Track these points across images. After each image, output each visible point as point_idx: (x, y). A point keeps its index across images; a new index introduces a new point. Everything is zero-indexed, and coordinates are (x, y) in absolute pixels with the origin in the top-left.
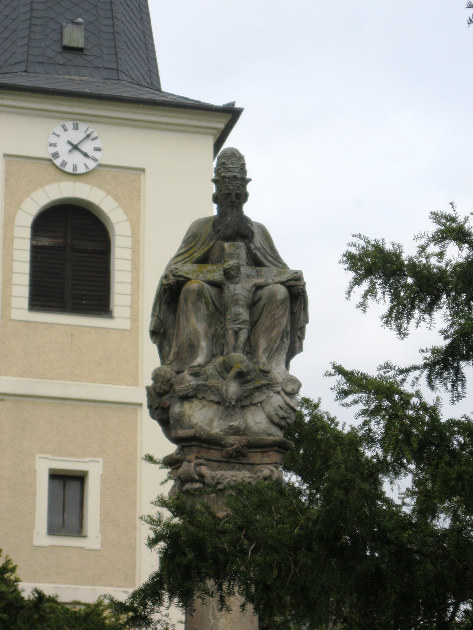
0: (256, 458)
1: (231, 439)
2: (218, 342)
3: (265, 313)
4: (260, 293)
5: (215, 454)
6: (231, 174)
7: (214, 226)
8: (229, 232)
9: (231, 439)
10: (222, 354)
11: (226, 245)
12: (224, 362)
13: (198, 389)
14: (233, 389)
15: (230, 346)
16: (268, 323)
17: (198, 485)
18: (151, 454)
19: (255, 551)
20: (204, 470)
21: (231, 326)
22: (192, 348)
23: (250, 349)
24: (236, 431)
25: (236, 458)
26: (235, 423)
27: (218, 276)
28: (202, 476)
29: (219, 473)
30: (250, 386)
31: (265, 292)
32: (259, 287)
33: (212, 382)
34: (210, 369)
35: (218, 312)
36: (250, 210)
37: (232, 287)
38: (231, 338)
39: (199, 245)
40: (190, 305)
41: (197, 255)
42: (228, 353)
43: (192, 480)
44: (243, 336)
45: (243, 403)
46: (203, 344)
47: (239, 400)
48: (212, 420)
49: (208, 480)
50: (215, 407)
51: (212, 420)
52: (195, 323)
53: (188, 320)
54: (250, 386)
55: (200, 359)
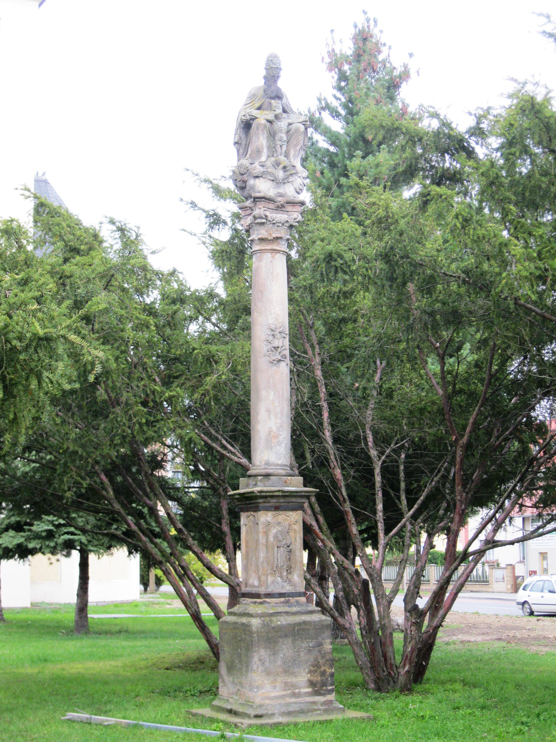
0: (289, 208)
1: (279, 199)
2: (272, 150)
3: (293, 137)
4: (290, 127)
5: (271, 206)
6: (275, 66)
7: (265, 91)
8: (273, 95)
9: (279, 199)
10: (273, 156)
11: (273, 101)
12: (276, 160)
13: (263, 173)
14: (281, 174)
15: (279, 153)
16: (295, 143)
17: (264, 221)
18: (194, 200)
19: (359, 260)
20: (268, 213)
21: (279, 143)
22: (259, 152)
23: (287, 155)
24: (281, 195)
25: (281, 208)
26: (280, 191)
27: (271, 117)
28: (266, 216)
29: (274, 215)
30: (288, 173)
31: (293, 126)
32: (290, 124)
33: (270, 170)
34: (269, 163)
35: (272, 135)
36: (281, 84)
37: (279, 123)
38: (279, 149)
39: (257, 100)
40: (260, 131)
41: (257, 105)
42: (277, 156)
43: (262, 218)
44: (284, 148)
45: (285, 181)
46: (265, 150)
47: (283, 180)
48: (269, 189)
49: (269, 218)
50: (271, 182)
51: (269, 189)
52: (260, 140)
53: (258, 138)
54: (288, 173)
55: (263, 158)
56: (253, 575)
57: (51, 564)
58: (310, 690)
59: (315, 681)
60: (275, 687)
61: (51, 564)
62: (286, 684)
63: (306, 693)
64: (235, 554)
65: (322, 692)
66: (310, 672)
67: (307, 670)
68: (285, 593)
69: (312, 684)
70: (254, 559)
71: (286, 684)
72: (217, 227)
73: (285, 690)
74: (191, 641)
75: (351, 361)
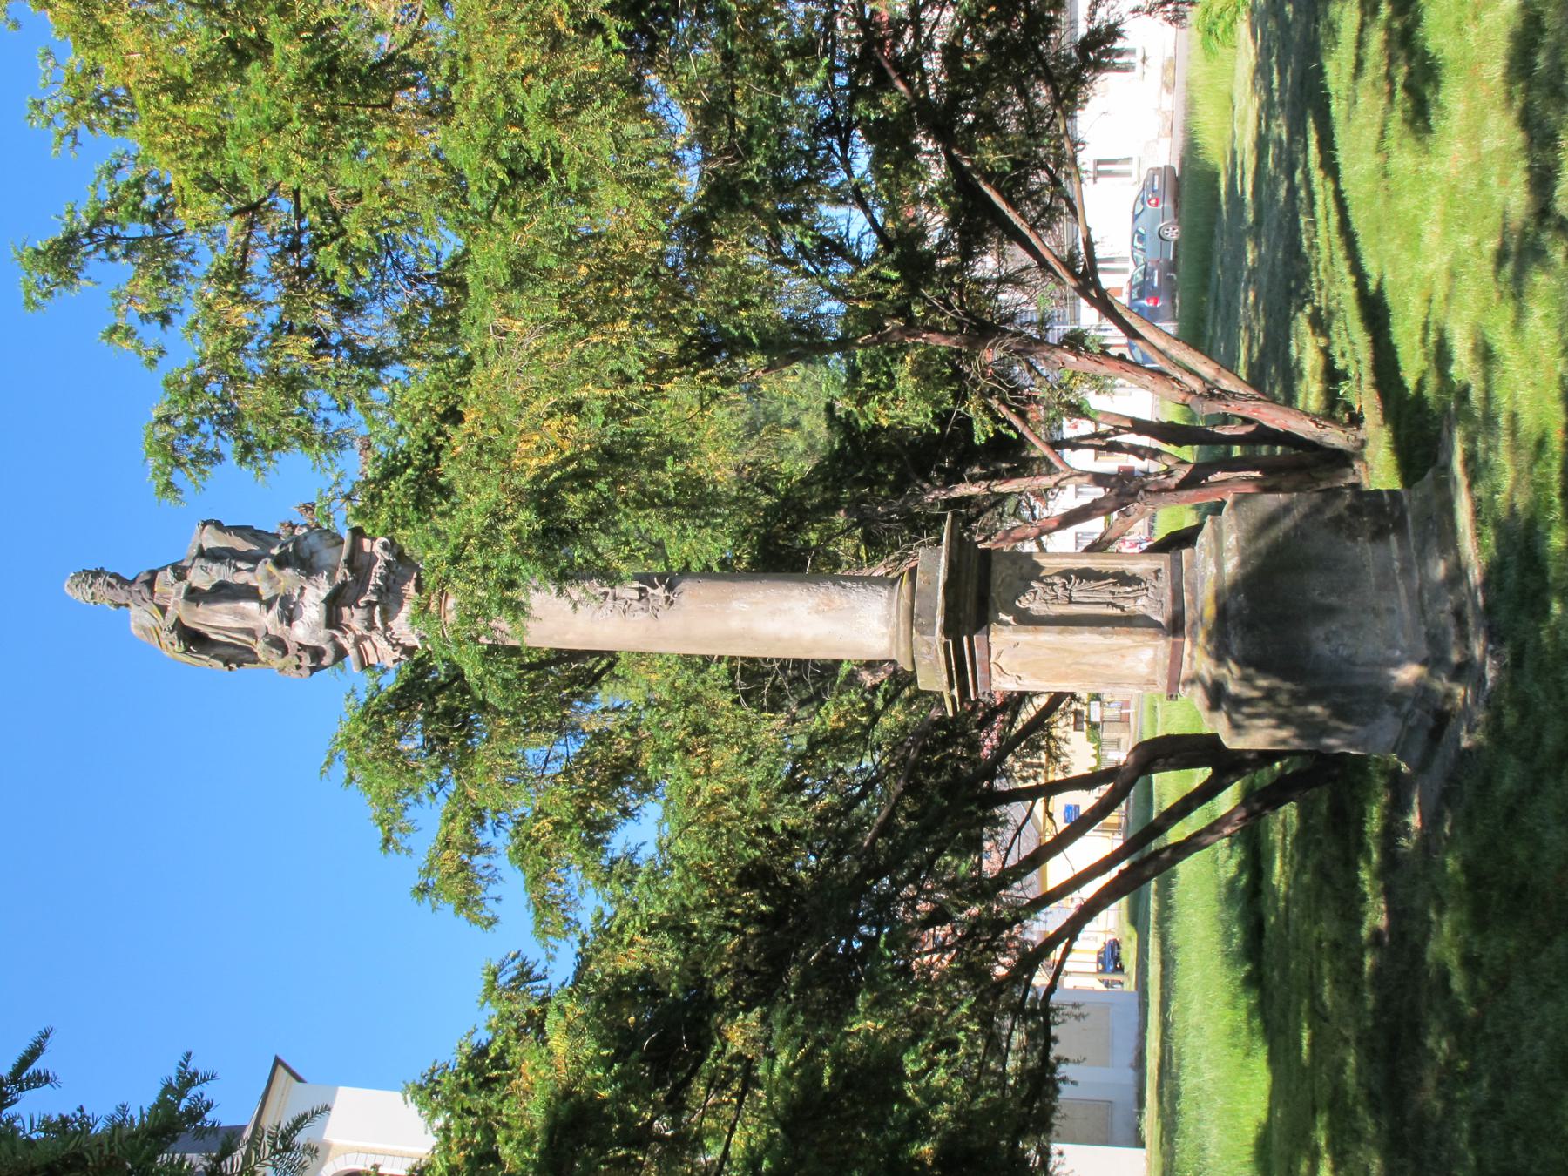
56: (1129, 662)
57: (161, 352)
58: (1393, 538)
59: (1375, 528)
60: (1391, 611)
61: (161, 352)
62: (1381, 587)
63: (1401, 547)
64: (1314, 1117)
65: (1397, 514)
66: (1353, 537)
67: (1349, 544)
68: (1173, 590)
69: (1379, 535)
70: (1093, 659)
71: (1381, 587)
72: (490, 904)
73: (1397, 590)
74: (1211, 569)
75: (271, 46)
